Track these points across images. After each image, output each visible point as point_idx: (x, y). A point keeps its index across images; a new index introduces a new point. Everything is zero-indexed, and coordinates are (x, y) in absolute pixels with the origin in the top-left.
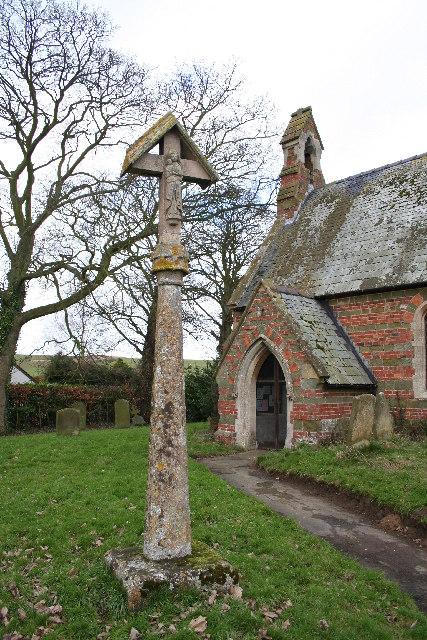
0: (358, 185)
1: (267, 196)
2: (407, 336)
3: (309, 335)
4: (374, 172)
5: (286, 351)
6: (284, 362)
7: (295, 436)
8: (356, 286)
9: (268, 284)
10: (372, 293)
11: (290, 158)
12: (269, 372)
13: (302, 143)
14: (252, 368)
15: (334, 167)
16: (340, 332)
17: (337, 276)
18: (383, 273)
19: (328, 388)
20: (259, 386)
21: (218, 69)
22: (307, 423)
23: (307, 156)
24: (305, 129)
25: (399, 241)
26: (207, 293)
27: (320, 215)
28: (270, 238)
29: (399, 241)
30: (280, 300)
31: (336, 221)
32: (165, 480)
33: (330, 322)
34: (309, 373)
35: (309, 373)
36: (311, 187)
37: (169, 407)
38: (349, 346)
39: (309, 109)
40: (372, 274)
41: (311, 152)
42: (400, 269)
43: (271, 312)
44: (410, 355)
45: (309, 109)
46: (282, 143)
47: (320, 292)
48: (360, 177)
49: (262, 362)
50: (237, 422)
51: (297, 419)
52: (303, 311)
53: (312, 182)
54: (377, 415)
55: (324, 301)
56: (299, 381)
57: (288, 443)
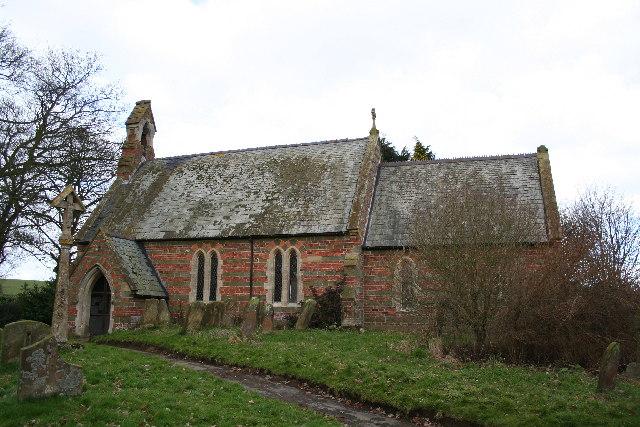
0: (175, 164)
1: (117, 150)
2: (188, 268)
3: (127, 263)
4: (188, 157)
5: (112, 274)
6: (110, 280)
7: (115, 326)
8: (161, 236)
9: (104, 231)
10: (170, 240)
11: (131, 136)
12: (100, 288)
13: (141, 127)
14: (89, 284)
15: (164, 146)
16: (149, 263)
17: (150, 229)
18: (178, 228)
19: (136, 296)
20: (93, 296)
21: (82, 55)
22: (122, 318)
23: (144, 136)
24: (144, 117)
25: (191, 210)
26: (51, 220)
27: (148, 181)
28: (110, 193)
29: (191, 210)
30: (112, 242)
31: (157, 187)
32: (61, 316)
33: (143, 257)
34: (126, 288)
35: (126, 288)
36: (144, 159)
37: (63, 291)
38: (154, 272)
39: (149, 102)
40: (170, 228)
41: (148, 131)
42: (188, 228)
43: (104, 248)
44: (189, 279)
45: (149, 102)
46: (127, 124)
47: (139, 237)
48: (177, 159)
49: (314, 154)
50: (77, 319)
51: (116, 317)
52: (126, 250)
53: (144, 155)
54: (160, 311)
55: (141, 243)
56: (120, 292)
57: (110, 331)
